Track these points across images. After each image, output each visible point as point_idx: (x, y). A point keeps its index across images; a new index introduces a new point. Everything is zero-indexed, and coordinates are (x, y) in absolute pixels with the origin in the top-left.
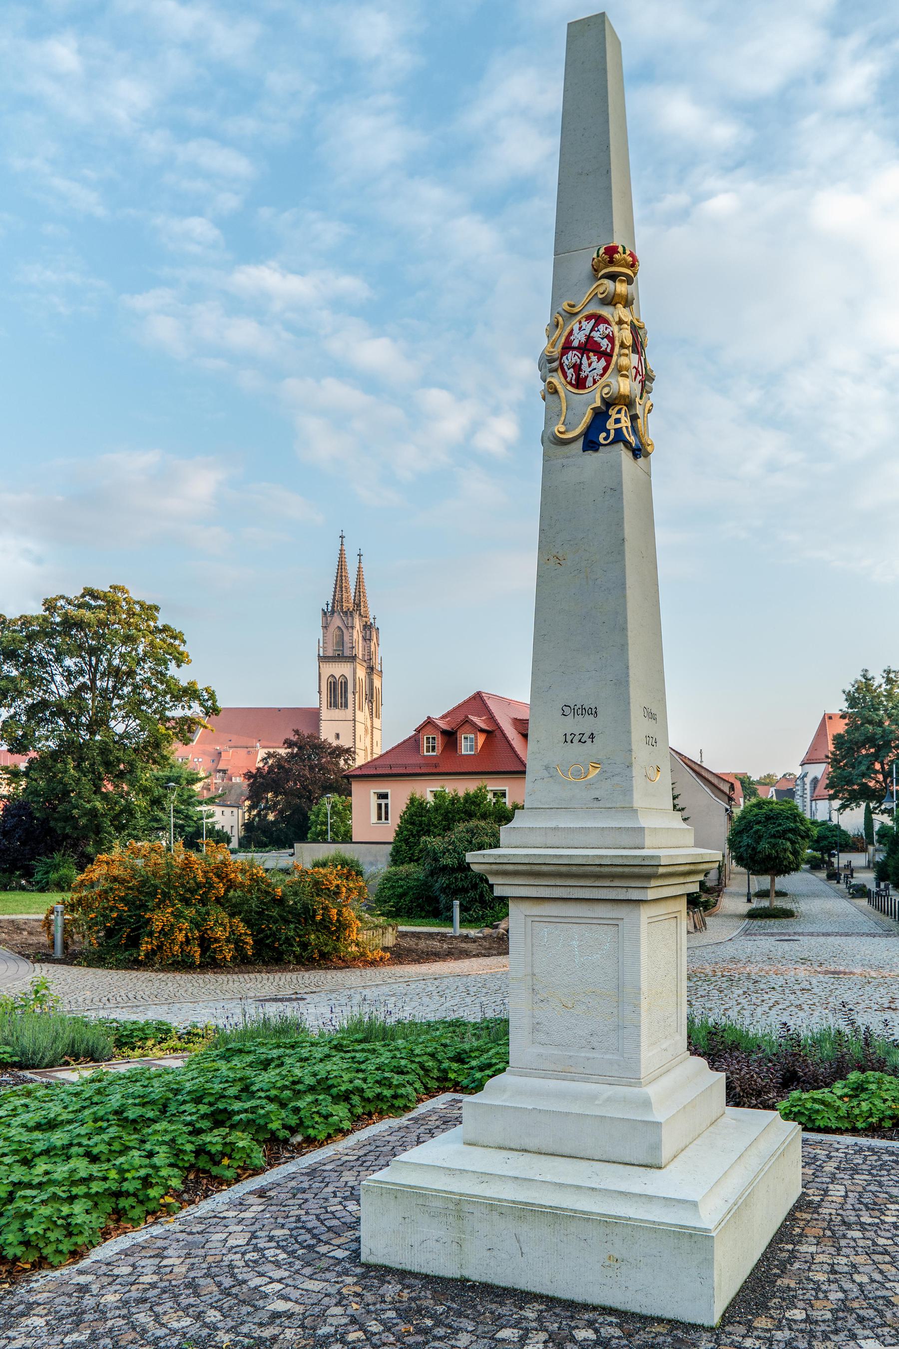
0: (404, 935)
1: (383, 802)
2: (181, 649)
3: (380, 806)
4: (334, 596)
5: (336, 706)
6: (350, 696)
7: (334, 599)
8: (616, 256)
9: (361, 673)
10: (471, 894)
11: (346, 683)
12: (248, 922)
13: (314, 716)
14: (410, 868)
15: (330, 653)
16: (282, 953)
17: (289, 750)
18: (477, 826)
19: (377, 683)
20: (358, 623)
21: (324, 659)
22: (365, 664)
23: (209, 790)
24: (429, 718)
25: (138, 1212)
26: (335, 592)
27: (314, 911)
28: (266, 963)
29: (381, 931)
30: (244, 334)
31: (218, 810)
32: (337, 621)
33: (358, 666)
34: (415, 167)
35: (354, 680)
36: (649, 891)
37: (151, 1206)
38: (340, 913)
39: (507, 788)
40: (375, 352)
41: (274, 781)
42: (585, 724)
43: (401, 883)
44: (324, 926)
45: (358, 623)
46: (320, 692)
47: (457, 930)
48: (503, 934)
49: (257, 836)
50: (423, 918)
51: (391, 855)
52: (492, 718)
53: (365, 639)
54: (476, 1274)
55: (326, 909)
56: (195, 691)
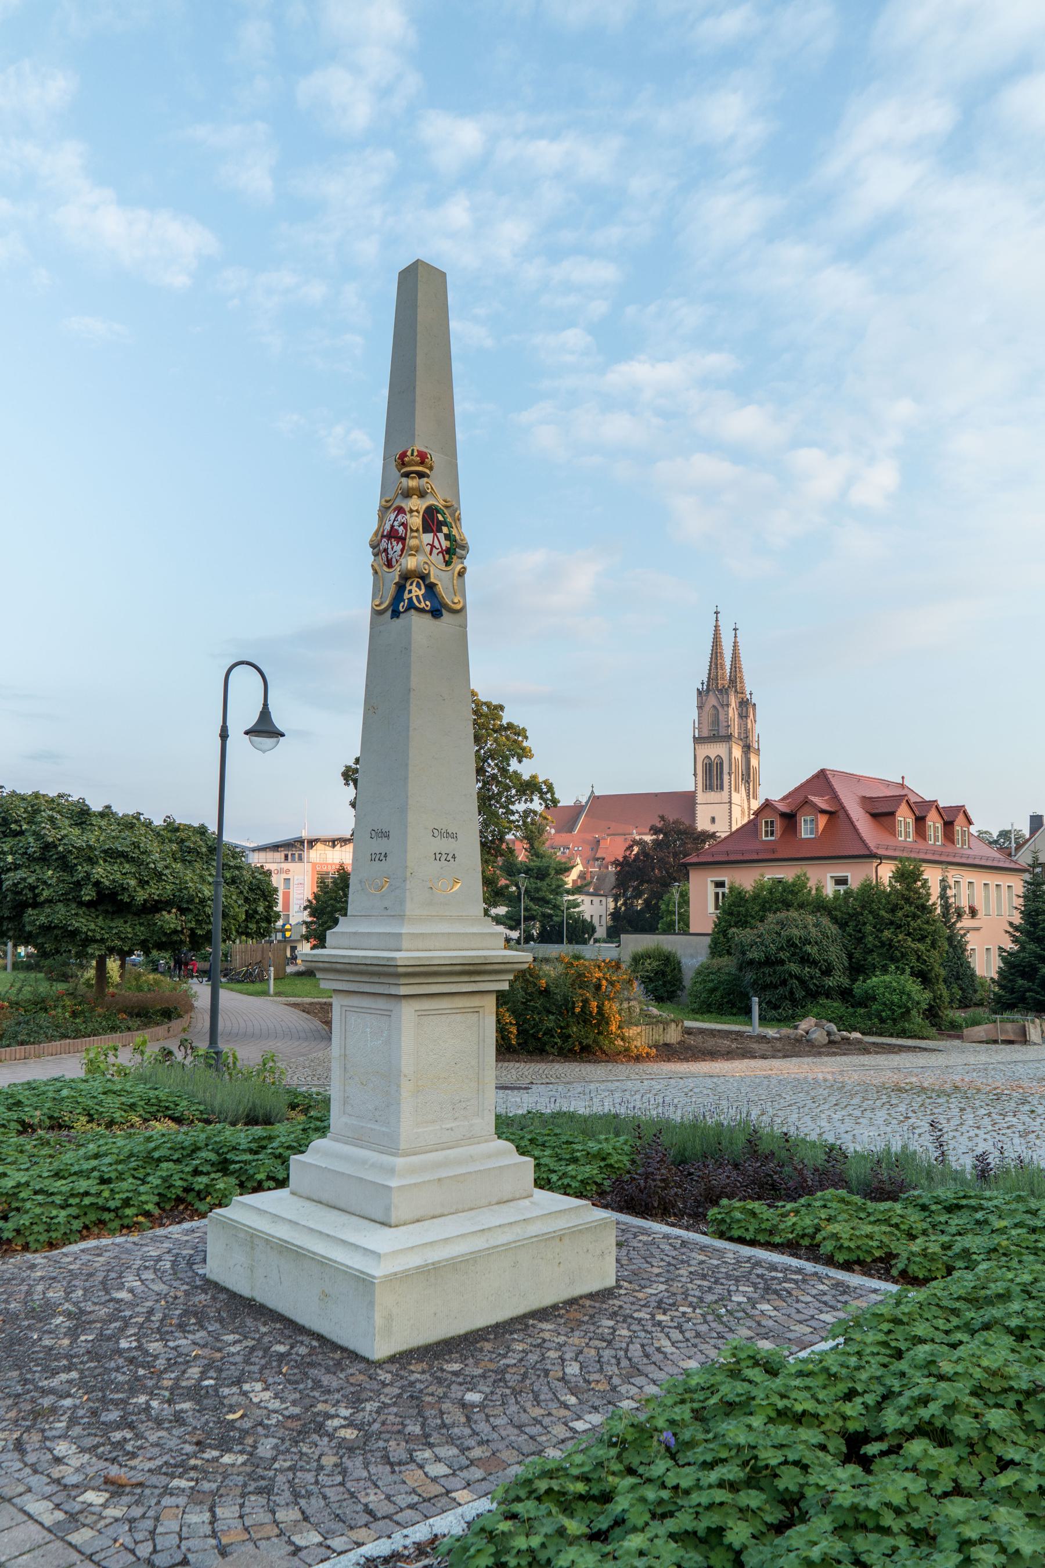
0: (688, 1032)
1: (720, 890)
2: (525, 744)
3: (717, 894)
4: (709, 674)
5: (711, 789)
6: (726, 777)
7: (709, 678)
8: (406, 459)
9: (737, 752)
10: (781, 990)
11: (722, 764)
12: (514, 1012)
13: (688, 800)
14: (725, 960)
15: (705, 734)
16: (545, 1044)
17: (654, 837)
18: (787, 918)
19: (754, 762)
20: (733, 701)
21: (698, 740)
22: (741, 743)
23: (585, 878)
24: (767, 800)
25: (116, 1224)
26: (710, 670)
27: (574, 1003)
28: (530, 1053)
29: (661, 1026)
30: (618, 427)
31: (587, 899)
32: (712, 700)
33: (734, 746)
34: (773, 232)
35: (730, 760)
36: (402, 987)
37: (126, 1222)
38: (600, 1008)
39: (849, 874)
40: (746, 422)
41: (639, 869)
42: (445, 845)
43: (712, 977)
44: (584, 1018)
45: (733, 701)
46: (695, 775)
47: (756, 1028)
48: (802, 1036)
49: (623, 923)
50: (735, 1015)
51: (710, 947)
52: (835, 798)
53: (741, 716)
54: (261, 1297)
55: (586, 1002)
56: (535, 785)
